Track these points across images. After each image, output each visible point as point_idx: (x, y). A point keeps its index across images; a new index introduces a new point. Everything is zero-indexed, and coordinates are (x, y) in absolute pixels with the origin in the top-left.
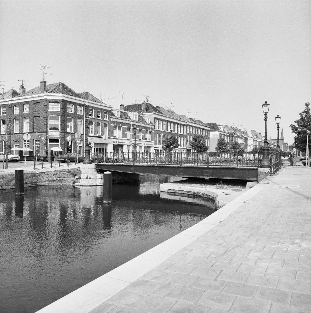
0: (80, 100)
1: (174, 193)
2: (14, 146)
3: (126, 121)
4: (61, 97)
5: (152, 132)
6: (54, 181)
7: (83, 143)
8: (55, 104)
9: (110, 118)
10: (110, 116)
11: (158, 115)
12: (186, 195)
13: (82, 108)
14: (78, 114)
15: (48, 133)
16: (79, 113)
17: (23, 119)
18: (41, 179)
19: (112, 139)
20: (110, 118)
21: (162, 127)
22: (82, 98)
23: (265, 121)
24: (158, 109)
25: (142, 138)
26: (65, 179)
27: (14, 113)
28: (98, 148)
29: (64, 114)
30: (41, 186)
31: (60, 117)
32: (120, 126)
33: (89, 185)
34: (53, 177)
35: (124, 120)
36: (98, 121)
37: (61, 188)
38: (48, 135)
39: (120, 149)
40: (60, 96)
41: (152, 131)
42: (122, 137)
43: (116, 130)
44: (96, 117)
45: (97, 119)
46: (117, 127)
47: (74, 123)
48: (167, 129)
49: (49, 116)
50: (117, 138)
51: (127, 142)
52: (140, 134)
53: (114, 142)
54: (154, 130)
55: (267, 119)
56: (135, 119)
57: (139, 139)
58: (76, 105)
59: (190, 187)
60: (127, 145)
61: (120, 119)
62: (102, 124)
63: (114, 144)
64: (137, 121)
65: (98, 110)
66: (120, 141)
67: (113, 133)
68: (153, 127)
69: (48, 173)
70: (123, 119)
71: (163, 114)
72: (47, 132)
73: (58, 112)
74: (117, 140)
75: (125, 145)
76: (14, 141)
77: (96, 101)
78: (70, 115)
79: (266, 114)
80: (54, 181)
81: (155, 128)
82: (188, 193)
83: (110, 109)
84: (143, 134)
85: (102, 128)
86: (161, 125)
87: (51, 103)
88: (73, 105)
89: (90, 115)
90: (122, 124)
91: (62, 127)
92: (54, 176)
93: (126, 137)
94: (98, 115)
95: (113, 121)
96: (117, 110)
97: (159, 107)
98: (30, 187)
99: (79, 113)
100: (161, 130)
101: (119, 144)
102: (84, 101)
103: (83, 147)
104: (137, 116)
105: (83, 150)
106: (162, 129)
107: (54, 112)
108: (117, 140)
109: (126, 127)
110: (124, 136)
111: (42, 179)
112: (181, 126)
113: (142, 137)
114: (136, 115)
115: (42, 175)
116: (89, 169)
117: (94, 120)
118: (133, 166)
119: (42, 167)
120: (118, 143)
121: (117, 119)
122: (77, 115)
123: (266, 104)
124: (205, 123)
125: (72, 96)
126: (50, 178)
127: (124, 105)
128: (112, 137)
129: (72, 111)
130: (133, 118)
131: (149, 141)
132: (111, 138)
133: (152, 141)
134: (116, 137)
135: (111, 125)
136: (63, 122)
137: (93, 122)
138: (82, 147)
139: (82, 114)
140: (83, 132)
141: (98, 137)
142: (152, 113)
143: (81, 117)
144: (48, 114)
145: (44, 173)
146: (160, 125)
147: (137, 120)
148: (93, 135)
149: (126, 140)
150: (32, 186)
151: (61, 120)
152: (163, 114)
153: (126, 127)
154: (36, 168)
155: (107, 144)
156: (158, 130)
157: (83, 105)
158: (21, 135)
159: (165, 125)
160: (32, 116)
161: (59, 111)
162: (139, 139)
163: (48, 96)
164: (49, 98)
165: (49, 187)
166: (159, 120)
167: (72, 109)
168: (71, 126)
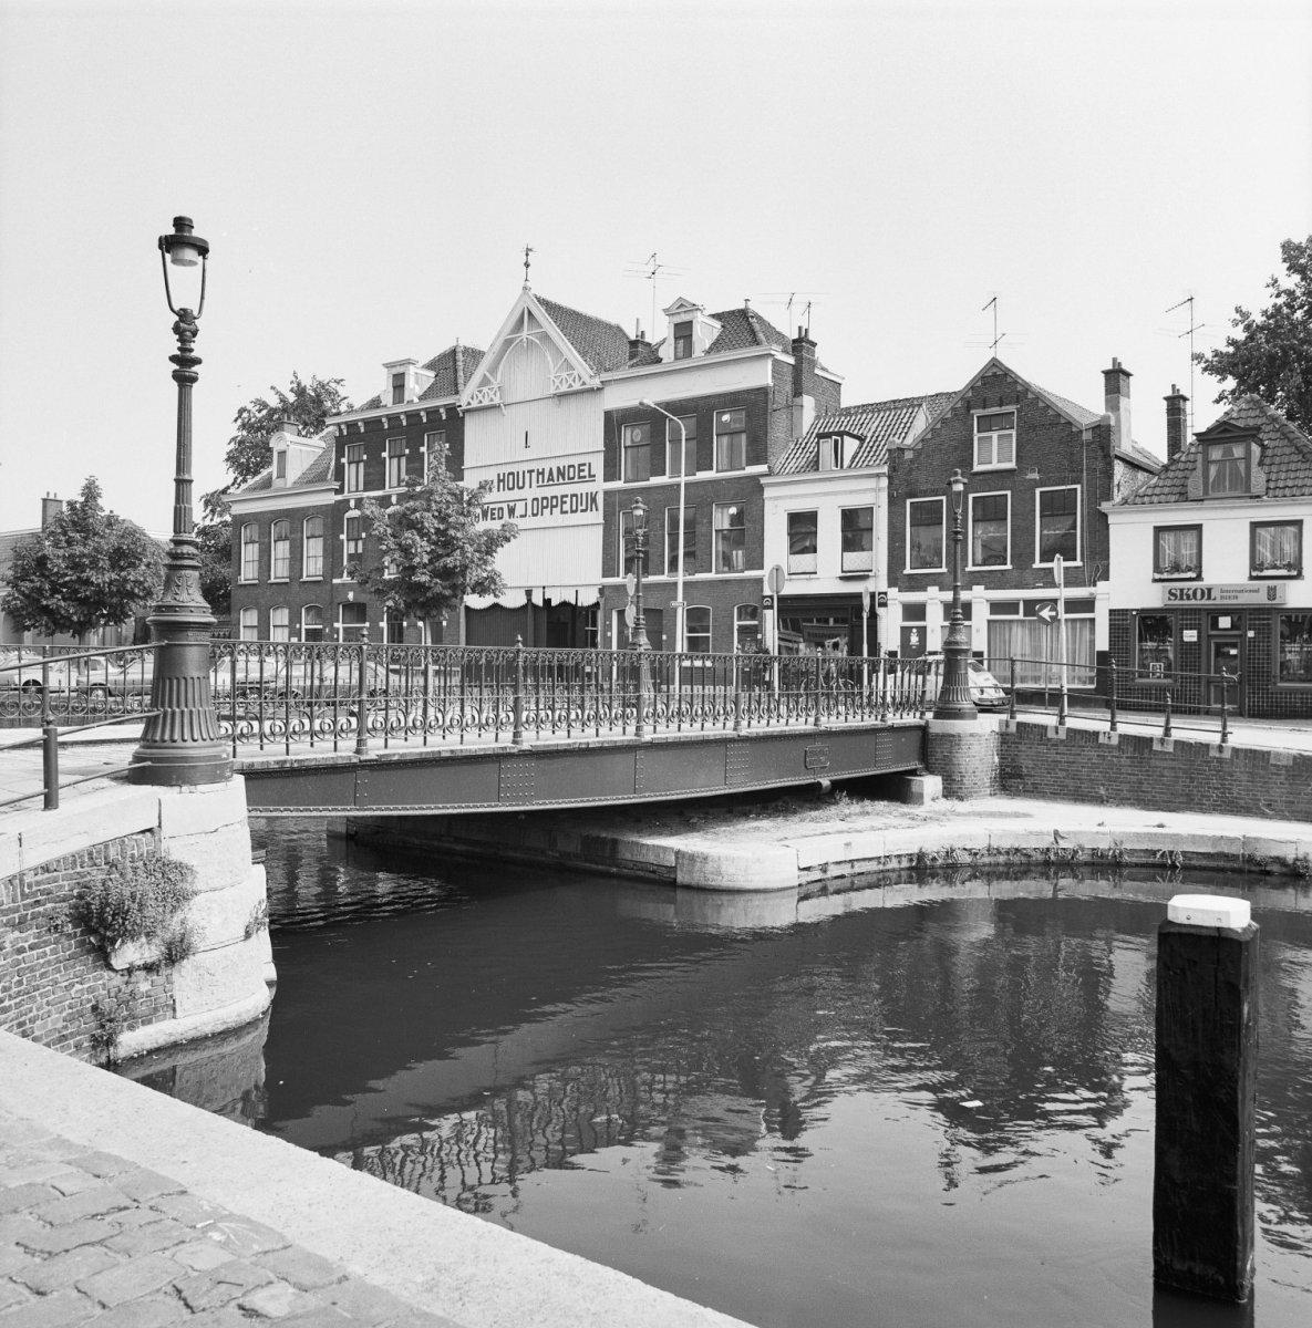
1: (820, 880)
12: (875, 876)
23: (174, 386)
55: (196, 368)
59: (1006, 828)
79: (185, 327)
82: (881, 867)
118: (732, 740)
123: (180, 240)
124: (1204, 430)
131: (551, 483)
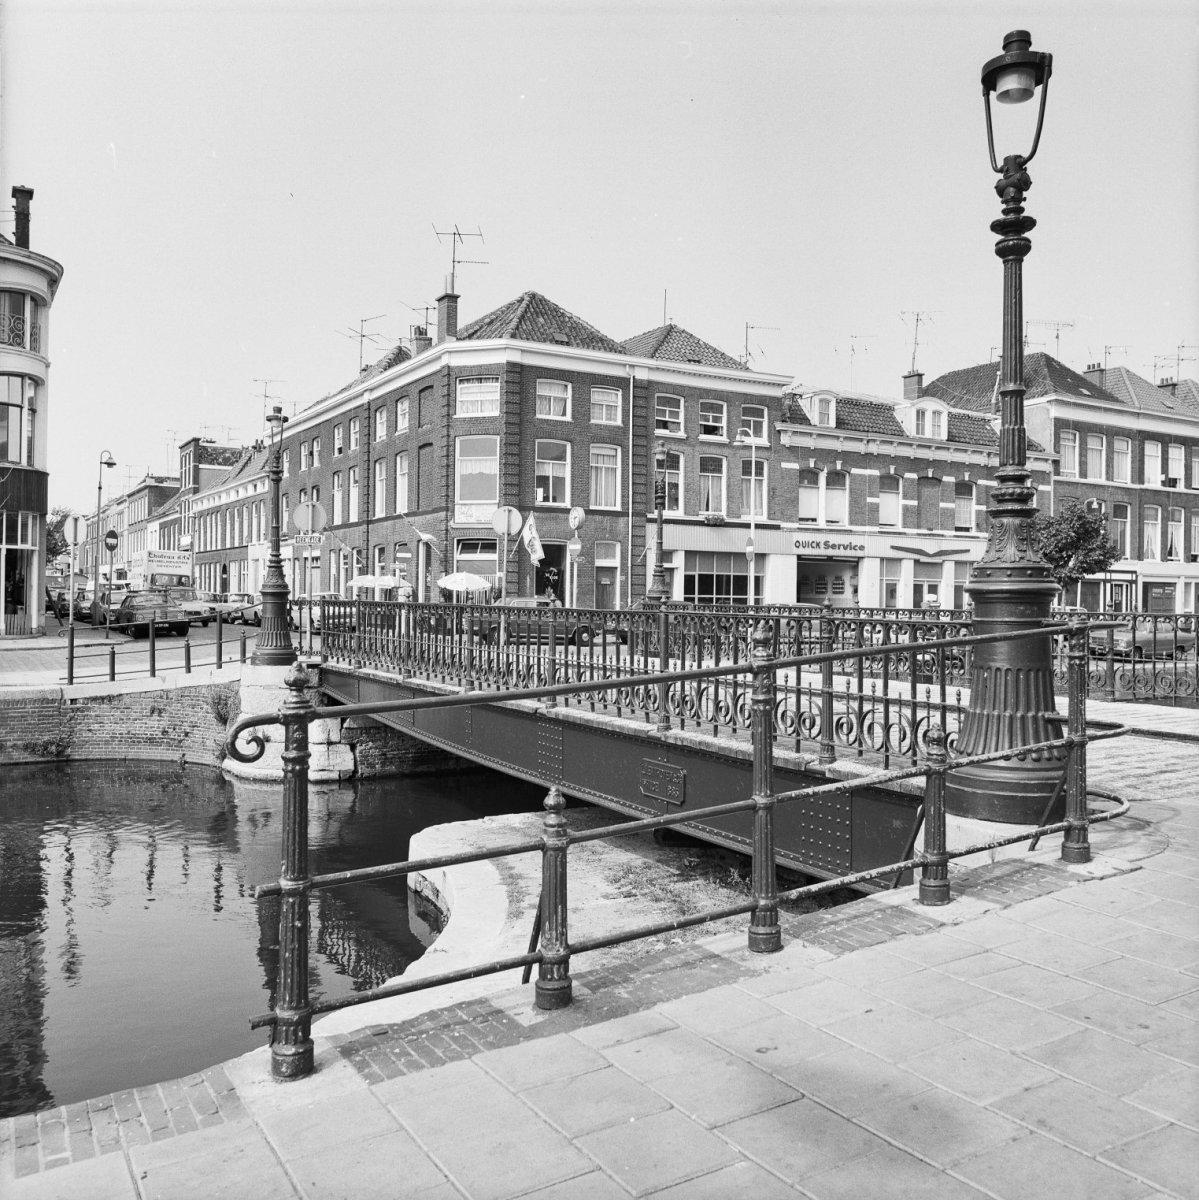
0: (543, 354)
2: (356, 572)
3: (871, 445)
4: (502, 353)
5: (1043, 492)
6: (151, 740)
7: (622, 553)
8: (484, 384)
9: (775, 434)
10: (779, 426)
11: (1076, 405)
13: (620, 393)
14: (592, 421)
15: (453, 511)
16: (599, 419)
17: (396, 460)
18: (90, 730)
19: (791, 530)
20: (779, 432)
21: (1108, 466)
22: (620, 352)
24: (1094, 379)
25: (973, 525)
26: (197, 734)
27: (378, 437)
28: (729, 576)
29: (520, 424)
30: (86, 760)
31: (501, 441)
32: (839, 467)
33: (258, 777)
34: (150, 723)
35: (861, 440)
36: (705, 449)
37: (178, 778)
38: (451, 523)
39: (847, 577)
40: (500, 351)
41: (1041, 488)
42: (852, 523)
43: (814, 491)
44: (698, 429)
45: (703, 443)
46: (823, 478)
47: (573, 464)
48: (1139, 474)
49: (458, 440)
50: (821, 524)
51: (882, 546)
52: (962, 503)
53: (798, 544)
54: (1057, 482)
56: (928, 434)
57: (958, 529)
58: (584, 382)
60: (882, 559)
61: (838, 437)
62: (728, 465)
63: (799, 557)
64: (941, 442)
65: (708, 401)
66: (834, 539)
67: (794, 502)
68: (1048, 467)
69: (127, 700)
70: (857, 435)
71: (1116, 400)
72: (449, 509)
73: (492, 419)
74: (821, 538)
75: (866, 560)
76: (377, 551)
77: (699, 362)
78: (552, 429)
80: (151, 740)
81: (1057, 473)
83: (777, 393)
84: (978, 503)
85: (729, 479)
86: (1077, 449)
87: (466, 385)
88: (570, 386)
89: (664, 425)
90: (849, 458)
91: (506, 485)
92: (155, 716)
93: (874, 521)
94: (711, 423)
95: (792, 449)
96: (820, 397)
97: (1102, 371)
98: (21, 764)
99: (599, 419)
100: (1102, 481)
101: (830, 552)
102: (625, 365)
103: (624, 572)
104: (944, 420)
105: (624, 585)
106: (1110, 476)
107: (477, 419)
108: (821, 538)
109: (876, 473)
110: (863, 513)
111: (96, 726)
112: (1093, 443)
113: (977, 518)
114: (936, 413)
115: (97, 709)
116: (267, 693)
117: (681, 448)
119: (66, 676)
120: (822, 552)
121: (819, 435)
122: (589, 426)
125: (568, 344)
126: (139, 728)
127: (920, 376)
128: (789, 519)
129: (564, 414)
130: (920, 428)
132: (783, 525)
133: (854, 528)
134: (814, 520)
135: (784, 465)
136: (511, 459)
137: (721, 460)
138: (619, 569)
139: (619, 422)
140: (624, 504)
141: (708, 525)
142: (1044, 399)
143: (614, 437)
144: (452, 433)
145: (110, 698)
146: (1091, 458)
147: (944, 436)
148: (679, 513)
149: (871, 534)
150: (32, 763)
151: (505, 454)
152: (1116, 400)
153: (876, 473)
154: (116, 671)
155: (761, 557)
156: (1083, 481)
157: (620, 383)
158: (390, 522)
159: (1130, 455)
160: (415, 445)
161: (496, 413)
162: (958, 529)
163: (453, 355)
164: (456, 361)
165: (133, 772)
166: (1084, 429)
167: (565, 400)
168: (559, 481)
